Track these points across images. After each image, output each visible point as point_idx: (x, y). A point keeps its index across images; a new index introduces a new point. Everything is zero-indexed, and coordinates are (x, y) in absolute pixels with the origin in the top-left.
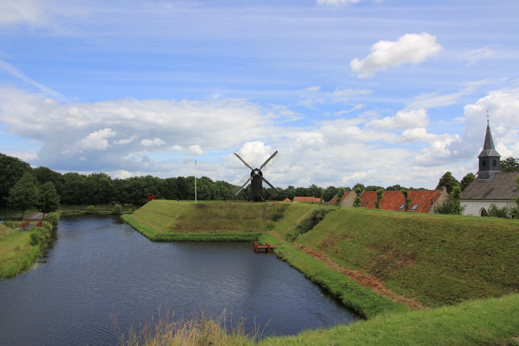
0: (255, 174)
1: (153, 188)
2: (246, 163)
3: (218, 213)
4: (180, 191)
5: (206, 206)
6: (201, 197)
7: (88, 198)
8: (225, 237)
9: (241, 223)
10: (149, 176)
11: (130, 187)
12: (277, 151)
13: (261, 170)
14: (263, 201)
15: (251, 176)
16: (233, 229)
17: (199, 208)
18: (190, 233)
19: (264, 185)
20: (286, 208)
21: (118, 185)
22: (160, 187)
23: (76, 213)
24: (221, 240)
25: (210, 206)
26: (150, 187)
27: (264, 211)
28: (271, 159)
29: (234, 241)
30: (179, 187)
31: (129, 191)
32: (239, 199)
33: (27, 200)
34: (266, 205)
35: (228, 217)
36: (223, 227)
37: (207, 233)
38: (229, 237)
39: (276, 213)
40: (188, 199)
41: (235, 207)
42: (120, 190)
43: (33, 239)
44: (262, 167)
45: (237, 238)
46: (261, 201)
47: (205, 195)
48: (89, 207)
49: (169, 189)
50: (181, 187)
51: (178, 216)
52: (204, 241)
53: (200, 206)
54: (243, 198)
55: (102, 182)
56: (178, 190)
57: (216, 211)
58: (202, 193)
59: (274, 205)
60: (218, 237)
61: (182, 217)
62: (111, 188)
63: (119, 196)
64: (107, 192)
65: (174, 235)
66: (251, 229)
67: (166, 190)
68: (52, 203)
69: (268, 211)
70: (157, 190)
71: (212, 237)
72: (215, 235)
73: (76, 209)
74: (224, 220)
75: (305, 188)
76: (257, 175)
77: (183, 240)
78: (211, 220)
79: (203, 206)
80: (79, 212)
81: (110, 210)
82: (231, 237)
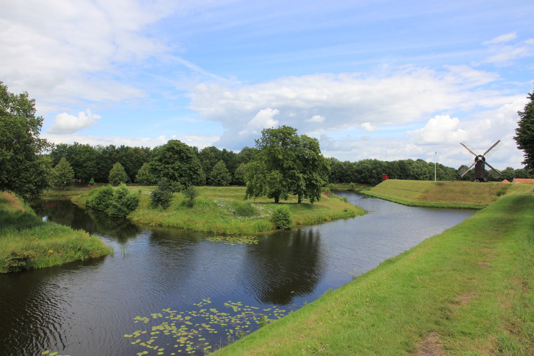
4: (402, 172)
5: (443, 184)
8: (461, 206)
9: (471, 197)
13: (484, 156)
14: (486, 182)
15: (475, 161)
16: (465, 201)
18: (434, 202)
19: (487, 168)
20: (509, 187)
21: (351, 168)
22: (385, 169)
25: (447, 185)
27: (490, 189)
29: (467, 208)
30: (401, 169)
31: (359, 172)
34: (492, 184)
35: (461, 192)
36: (457, 199)
37: (446, 203)
38: (463, 206)
39: (500, 190)
42: (351, 171)
44: (485, 154)
45: (470, 207)
46: (484, 181)
50: (402, 170)
51: (423, 190)
52: (445, 208)
53: (440, 184)
54: (456, 178)
55: (338, 165)
57: (452, 188)
59: (498, 185)
60: (455, 205)
61: (427, 192)
62: (344, 170)
63: (352, 176)
64: (342, 173)
65: (424, 203)
66: (479, 201)
69: (493, 189)
70: (382, 172)
71: (451, 205)
72: (453, 204)
74: (458, 194)
76: (481, 161)
79: (441, 184)
81: (347, 188)
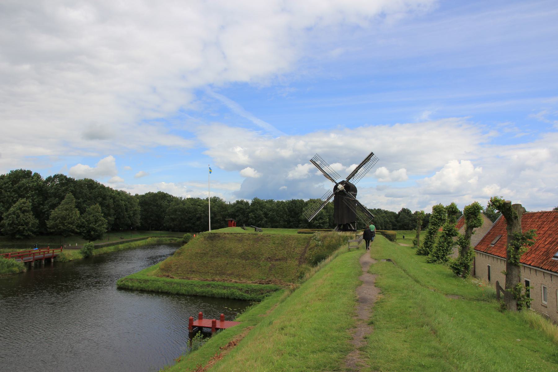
0: (339, 189)
1: (259, 212)
2: (327, 174)
3: (231, 249)
5: (219, 236)
6: (317, 224)
7: (190, 225)
8: (215, 291)
10: (282, 201)
11: (233, 212)
12: (372, 153)
16: (243, 276)
17: (207, 240)
23: (173, 241)
24: (207, 295)
25: (225, 238)
26: (256, 211)
27: (306, 248)
28: (362, 166)
32: (384, 227)
33: (64, 225)
36: (229, 272)
40: (225, 226)
41: (262, 238)
43: (163, 267)
47: (322, 223)
48: (185, 235)
49: (276, 214)
56: (289, 215)
58: (318, 219)
67: (273, 215)
68: (94, 229)
70: (263, 216)
73: (174, 237)
74: (236, 260)
75: (154, 192)
77: (154, 290)
78: (216, 259)
80: (176, 240)
82: (225, 291)
